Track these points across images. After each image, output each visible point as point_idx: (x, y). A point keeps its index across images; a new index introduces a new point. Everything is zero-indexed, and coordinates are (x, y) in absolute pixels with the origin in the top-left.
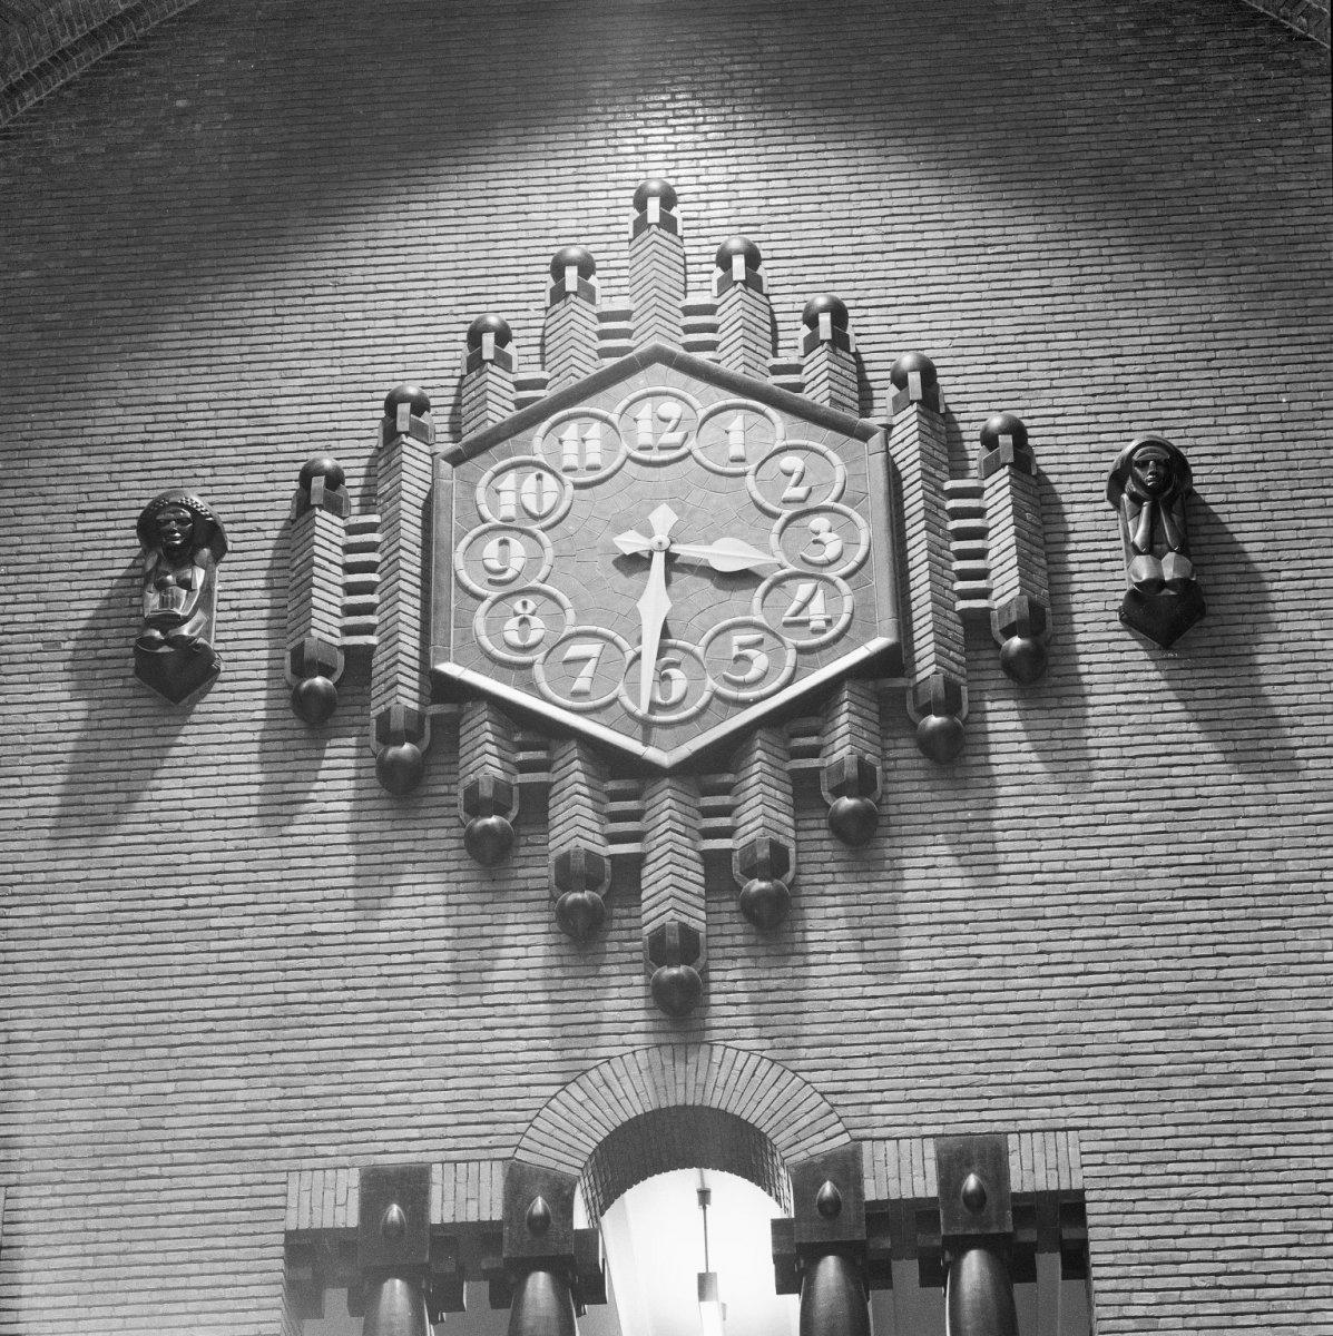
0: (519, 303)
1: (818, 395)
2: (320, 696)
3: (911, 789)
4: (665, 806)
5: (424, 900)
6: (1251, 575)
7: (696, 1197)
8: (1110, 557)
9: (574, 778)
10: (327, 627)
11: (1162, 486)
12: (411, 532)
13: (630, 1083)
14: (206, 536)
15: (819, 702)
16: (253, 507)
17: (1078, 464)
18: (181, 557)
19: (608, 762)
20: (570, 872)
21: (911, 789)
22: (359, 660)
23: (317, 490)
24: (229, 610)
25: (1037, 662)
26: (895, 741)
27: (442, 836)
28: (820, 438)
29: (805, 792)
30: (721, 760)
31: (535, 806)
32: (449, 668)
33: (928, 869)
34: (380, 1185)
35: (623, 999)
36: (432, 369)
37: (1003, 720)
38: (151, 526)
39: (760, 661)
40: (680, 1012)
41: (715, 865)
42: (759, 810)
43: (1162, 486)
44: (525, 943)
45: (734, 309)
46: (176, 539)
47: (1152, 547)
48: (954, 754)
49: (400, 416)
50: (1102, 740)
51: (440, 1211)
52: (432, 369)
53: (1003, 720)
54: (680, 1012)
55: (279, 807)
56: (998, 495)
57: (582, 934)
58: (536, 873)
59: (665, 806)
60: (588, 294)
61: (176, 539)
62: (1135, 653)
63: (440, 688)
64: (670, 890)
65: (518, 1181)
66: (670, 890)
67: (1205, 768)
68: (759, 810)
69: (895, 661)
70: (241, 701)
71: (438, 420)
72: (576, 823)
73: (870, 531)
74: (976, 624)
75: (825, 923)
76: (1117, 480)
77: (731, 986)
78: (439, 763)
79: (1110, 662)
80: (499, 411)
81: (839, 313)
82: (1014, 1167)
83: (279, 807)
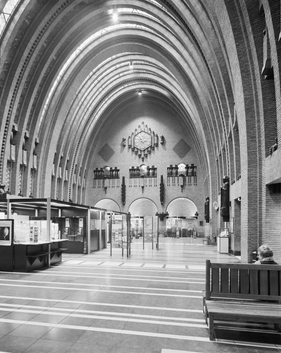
0: (137, 128)
1: (149, 133)
2: (130, 147)
3: (152, 151)
4: (142, 152)
5: (134, 155)
6: (166, 141)
7: (51, 178)
8: (160, 141)
9: (139, 151)
10: (130, 144)
11: (163, 138)
12: (133, 139)
13: (141, 163)
14: (125, 139)
15: (148, 148)
16: (127, 138)
17: (159, 136)
18: (124, 141)
19: (140, 150)
20: (136, 152)
21: (152, 151)
23: (129, 137)
24: (126, 143)
25: (157, 145)
26: (152, 148)
27: (134, 153)
28: (149, 135)
29: (148, 151)
30: (145, 150)
31: (138, 152)
32: (134, 146)
33: (152, 154)
34: (170, 166)
35: (141, 160)
36: (133, 131)
37: (156, 148)
38: (123, 139)
39: (146, 146)
40: (143, 160)
41: (144, 155)
42: (146, 152)
43: (163, 138)
44: (138, 157)
45: (146, 128)
46: (124, 140)
47: (162, 141)
48: (153, 150)
49: (133, 134)
50: (159, 149)
51: (134, 168)
52: (133, 131)
53: (156, 148)
54: (143, 160)
55: (128, 151)
56: (156, 138)
57: (140, 157)
58: (138, 154)
59: (142, 152)
60: (140, 127)
61: (124, 140)
62: (161, 145)
63: (134, 147)
65: (137, 167)
66: (143, 156)
67: (163, 150)
68: (146, 152)
69: (151, 146)
70: (127, 147)
71: (134, 134)
72: (139, 153)
73: (151, 140)
74: (155, 144)
75: (148, 157)
76: (161, 137)
77: (145, 159)
78: (134, 150)
79: (160, 145)
80: (136, 134)
81: (150, 129)
82: (58, 227)
83: (128, 151)
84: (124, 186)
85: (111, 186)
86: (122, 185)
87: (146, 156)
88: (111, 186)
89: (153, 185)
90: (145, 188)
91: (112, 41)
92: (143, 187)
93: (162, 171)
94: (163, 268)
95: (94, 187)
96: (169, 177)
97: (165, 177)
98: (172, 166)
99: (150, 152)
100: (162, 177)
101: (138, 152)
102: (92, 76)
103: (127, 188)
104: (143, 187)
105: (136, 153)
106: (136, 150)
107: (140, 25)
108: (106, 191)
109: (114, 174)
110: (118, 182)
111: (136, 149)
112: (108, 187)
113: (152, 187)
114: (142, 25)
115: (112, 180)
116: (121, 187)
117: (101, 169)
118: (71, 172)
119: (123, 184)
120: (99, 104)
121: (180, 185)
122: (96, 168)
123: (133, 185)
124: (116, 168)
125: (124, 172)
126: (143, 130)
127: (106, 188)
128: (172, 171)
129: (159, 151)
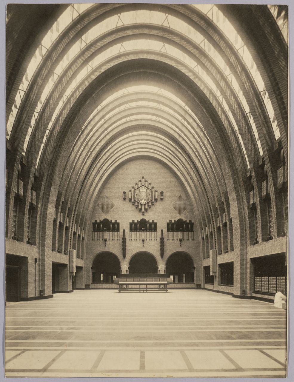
22: (131, 199)
29: (148, 206)
31: (138, 206)
40: (143, 214)
58: (138, 208)
64: (143, 210)
66: (143, 210)
68: (146, 207)
69: (151, 201)
72: (140, 207)
84: (124, 239)
85: (148, 238)
86: (123, 239)
87: (146, 210)
88: (111, 238)
89: (153, 239)
90: (145, 241)
91: (68, 122)
92: (143, 241)
93: (162, 225)
94: (105, 350)
95: (93, 240)
96: (94, 232)
97: (165, 230)
98: (97, 222)
99: (149, 207)
100: (162, 231)
101: (138, 206)
102: (130, 146)
103: (165, 240)
104: (143, 241)
105: (137, 207)
106: (136, 204)
107: (185, 120)
108: (106, 244)
109: (114, 227)
110: (118, 235)
111: (136, 203)
112: (108, 239)
113: (152, 241)
114: (186, 122)
115: (154, 232)
116: (121, 240)
117: (100, 221)
118: (72, 220)
119: (124, 237)
120: (93, 164)
121: (179, 240)
122: (152, 221)
123: (116, 238)
124: (116, 221)
125: (125, 226)
126: (143, 184)
127: (106, 240)
128: (173, 227)
129: (159, 206)
